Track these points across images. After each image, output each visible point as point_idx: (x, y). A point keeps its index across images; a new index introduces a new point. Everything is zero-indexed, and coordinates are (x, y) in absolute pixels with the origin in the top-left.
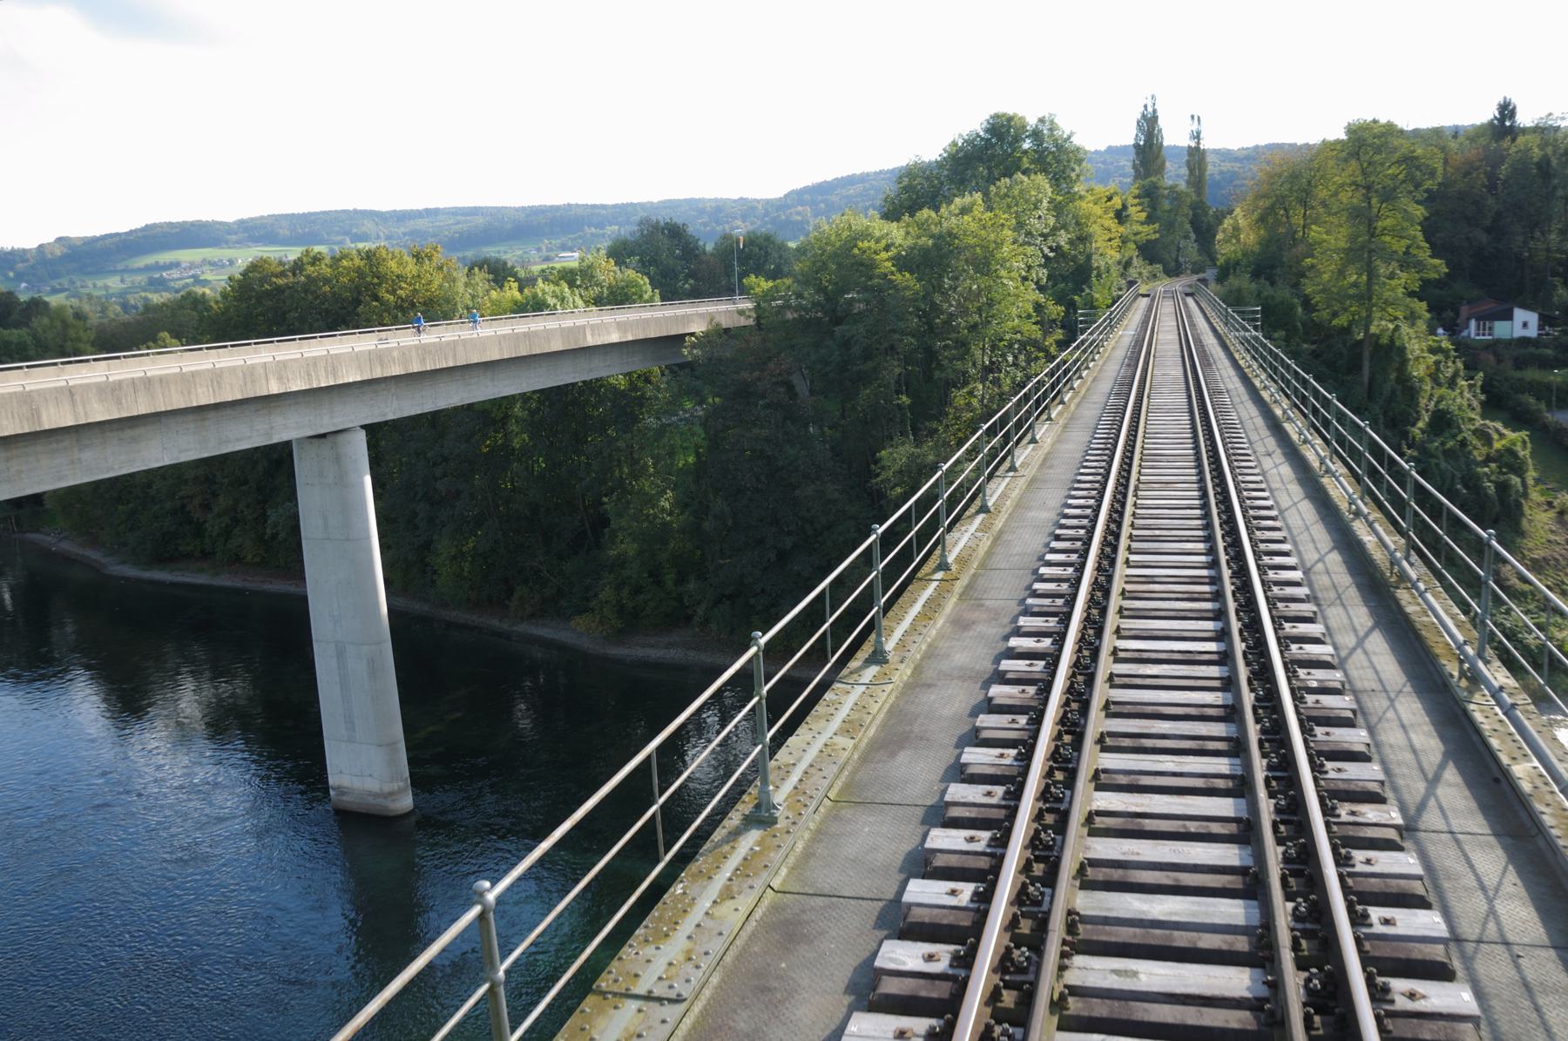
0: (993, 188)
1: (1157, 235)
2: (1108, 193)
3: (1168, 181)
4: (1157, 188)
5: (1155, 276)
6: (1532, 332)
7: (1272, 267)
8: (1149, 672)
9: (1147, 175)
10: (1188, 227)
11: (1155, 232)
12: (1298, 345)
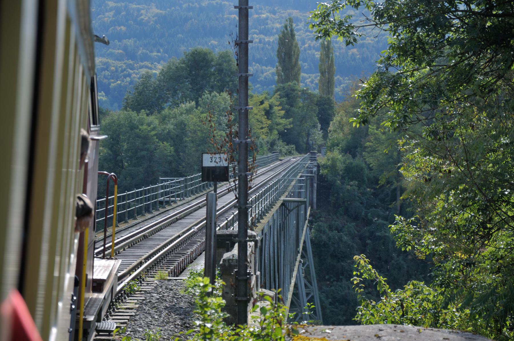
0: (200, 99)
1: (292, 126)
2: (261, 100)
3: (301, 86)
4: (294, 90)
5: (290, 152)
6: (103, 93)
7: (356, 147)
8: (283, 250)
9: (288, 78)
10: (316, 119)
11: (290, 124)
12: (365, 189)
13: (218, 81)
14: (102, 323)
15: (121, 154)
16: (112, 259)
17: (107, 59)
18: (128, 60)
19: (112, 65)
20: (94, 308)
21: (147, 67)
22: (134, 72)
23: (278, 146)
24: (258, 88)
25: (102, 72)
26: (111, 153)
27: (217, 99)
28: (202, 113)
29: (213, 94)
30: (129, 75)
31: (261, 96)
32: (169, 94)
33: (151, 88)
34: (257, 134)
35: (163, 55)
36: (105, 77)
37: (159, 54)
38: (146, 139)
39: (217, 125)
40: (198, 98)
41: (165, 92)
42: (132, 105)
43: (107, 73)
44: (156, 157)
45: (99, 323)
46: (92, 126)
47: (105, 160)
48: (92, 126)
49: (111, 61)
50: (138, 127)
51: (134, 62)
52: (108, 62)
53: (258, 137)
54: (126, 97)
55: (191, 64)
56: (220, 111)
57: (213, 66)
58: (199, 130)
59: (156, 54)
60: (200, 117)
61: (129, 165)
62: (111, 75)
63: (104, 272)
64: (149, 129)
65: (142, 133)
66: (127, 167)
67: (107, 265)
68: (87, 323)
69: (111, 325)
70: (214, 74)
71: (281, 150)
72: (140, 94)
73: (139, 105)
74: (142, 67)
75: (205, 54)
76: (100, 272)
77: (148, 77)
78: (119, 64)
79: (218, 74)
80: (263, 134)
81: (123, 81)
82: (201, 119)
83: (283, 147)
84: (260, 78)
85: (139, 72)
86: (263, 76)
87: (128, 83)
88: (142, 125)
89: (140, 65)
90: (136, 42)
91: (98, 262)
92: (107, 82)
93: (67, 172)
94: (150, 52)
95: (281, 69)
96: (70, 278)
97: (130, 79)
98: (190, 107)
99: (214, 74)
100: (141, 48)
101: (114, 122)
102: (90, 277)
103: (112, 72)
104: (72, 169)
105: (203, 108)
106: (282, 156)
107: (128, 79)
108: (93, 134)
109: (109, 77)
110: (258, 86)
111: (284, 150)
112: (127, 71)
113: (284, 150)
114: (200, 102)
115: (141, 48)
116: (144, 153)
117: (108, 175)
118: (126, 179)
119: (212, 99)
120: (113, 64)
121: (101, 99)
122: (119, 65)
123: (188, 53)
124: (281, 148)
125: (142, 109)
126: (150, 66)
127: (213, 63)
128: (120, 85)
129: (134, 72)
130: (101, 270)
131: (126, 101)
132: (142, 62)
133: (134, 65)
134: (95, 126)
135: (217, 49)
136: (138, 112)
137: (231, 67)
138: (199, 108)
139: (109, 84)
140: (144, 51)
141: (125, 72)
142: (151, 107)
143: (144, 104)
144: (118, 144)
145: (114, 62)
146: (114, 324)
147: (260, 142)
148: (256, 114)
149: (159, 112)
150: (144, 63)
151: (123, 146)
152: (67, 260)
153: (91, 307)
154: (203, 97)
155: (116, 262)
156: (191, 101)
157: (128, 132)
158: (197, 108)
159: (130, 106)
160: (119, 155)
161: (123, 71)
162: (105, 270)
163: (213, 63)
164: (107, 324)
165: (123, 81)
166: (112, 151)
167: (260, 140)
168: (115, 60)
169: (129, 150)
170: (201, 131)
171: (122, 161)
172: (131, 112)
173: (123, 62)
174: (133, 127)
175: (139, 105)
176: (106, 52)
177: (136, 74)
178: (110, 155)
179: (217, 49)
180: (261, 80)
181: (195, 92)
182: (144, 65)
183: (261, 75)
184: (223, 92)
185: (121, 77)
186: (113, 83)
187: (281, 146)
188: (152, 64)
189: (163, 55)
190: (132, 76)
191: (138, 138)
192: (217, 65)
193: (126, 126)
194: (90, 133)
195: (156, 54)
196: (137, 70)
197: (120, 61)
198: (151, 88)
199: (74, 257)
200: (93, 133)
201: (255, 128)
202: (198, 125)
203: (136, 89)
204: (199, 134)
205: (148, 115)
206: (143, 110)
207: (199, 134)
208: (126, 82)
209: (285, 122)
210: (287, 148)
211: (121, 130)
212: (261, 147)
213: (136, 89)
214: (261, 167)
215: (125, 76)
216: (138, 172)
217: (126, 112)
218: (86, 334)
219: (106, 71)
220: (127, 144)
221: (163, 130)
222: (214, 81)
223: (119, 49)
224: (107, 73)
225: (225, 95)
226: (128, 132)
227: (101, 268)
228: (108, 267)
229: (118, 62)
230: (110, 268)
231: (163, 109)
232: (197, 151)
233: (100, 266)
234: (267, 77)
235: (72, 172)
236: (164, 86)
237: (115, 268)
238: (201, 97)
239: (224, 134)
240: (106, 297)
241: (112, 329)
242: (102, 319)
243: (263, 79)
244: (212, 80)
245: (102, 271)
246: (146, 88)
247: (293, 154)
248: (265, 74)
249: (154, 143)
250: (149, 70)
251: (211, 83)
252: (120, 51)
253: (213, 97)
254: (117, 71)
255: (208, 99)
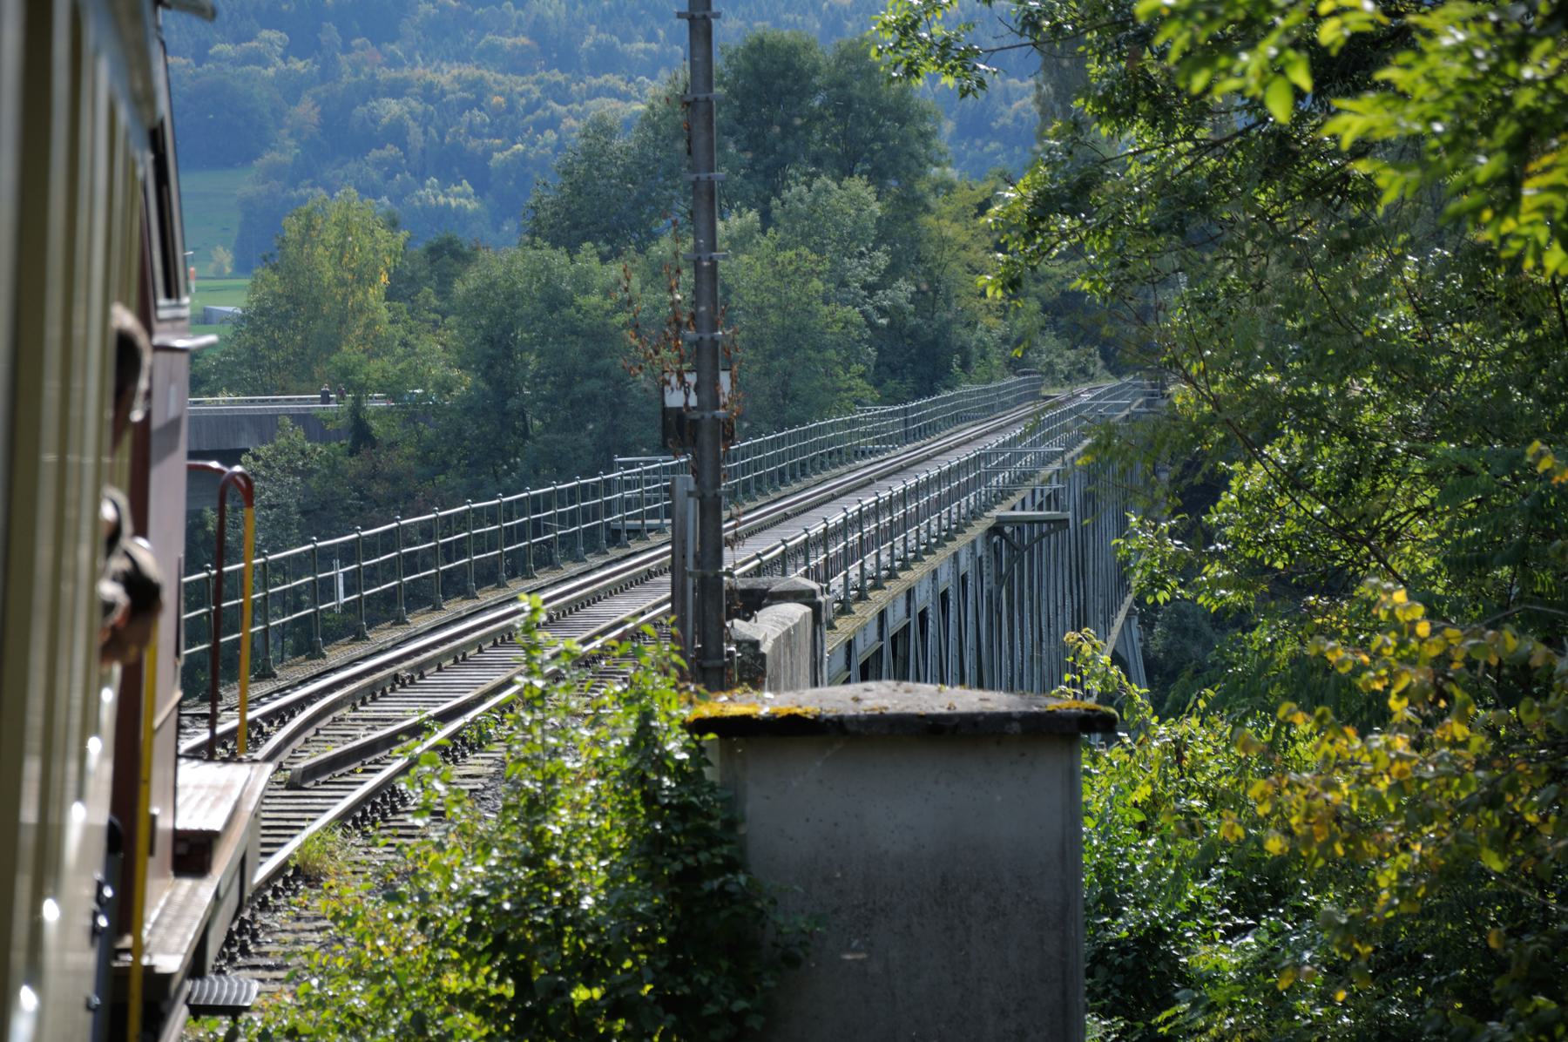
0: (775, 202)
2: (980, 199)
13: (835, 140)
14: (207, 984)
15: (521, 391)
16: (240, 761)
17: (478, 68)
18: (548, 68)
19: (496, 88)
20: (181, 930)
21: (613, 93)
22: (570, 111)
23: (1040, 352)
24: (994, 153)
25: (461, 113)
26: (487, 388)
27: (832, 201)
28: (782, 246)
29: (817, 184)
30: (553, 123)
31: (981, 187)
32: (674, 187)
33: (614, 170)
34: (967, 313)
35: (668, 50)
36: (473, 132)
37: (654, 46)
38: (598, 338)
39: (831, 285)
40: (767, 201)
41: (661, 179)
42: (552, 226)
43: (478, 116)
44: (635, 397)
45: (198, 983)
46: (162, 301)
47: (468, 410)
48: (162, 301)
49: (490, 75)
50: (572, 302)
51: (568, 75)
52: (482, 78)
53: (971, 325)
54: (531, 202)
55: (743, 87)
56: (840, 240)
57: (817, 90)
58: (771, 306)
59: (642, 45)
60: (774, 263)
61: (547, 427)
62: (492, 124)
63: (214, 806)
64: (608, 304)
65: (587, 321)
66: (540, 434)
67: (222, 782)
68: (158, 984)
69: (240, 988)
70: (821, 117)
71: (1050, 365)
72: (577, 189)
73: (575, 226)
74: (596, 93)
75: (792, 51)
76: (198, 806)
77: (602, 129)
78: (521, 84)
79: (835, 115)
80: (989, 311)
81: (534, 144)
82: (779, 267)
83: (1060, 356)
84: (1001, 121)
85: (586, 111)
86: (1011, 112)
87: (548, 150)
88: (586, 292)
89: (589, 87)
90: (575, 8)
91: (190, 772)
92: (480, 150)
93: (62, 464)
94: (622, 42)
95: (1051, 90)
96: (88, 829)
97: (555, 136)
98: (742, 229)
99: (821, 117)
100: (593, 28)
101: (492, 285)
102: (164, 824)
103: (496, 113)
104: (82, 453)
105: (786, 230)
106: (1054, 385)
107: (551, 136)
108: (165, 332)
109: (486, 130)
110: (993, 146)
111: (1062, 366)
112: (546, 108)
113: (1062, 366)
114: (776, 213)
115: (593, 28)
116: (594, 385)
117: (220, 472)
118: (536, 472)
119: (815, 201)
120: (499, 83)
121: (459, 207)
122: (519, 89)
123: (733, 48)
124: (1052, 356)
125: (585, 240)
126: (623, 87)
127: (817, 81)
128: (522, 159)
129: (570, 111)
130: (203, 799)
131: (533, 214)
132: (596, 76)
133: (568, 88)
134: (173, 302)
135: (850, 25)
136: (573, 250)
137: (879, 94)
138: (771, 230)
139: (488, 154)
140: (603, 37)
141: (539, 112)
142: (616, 232)
143: (593, 223)
144: (509, 357)
145: (500, 77)
146: (249, 985)
147: (980, 340)
148: (964, 247)
149: (641, 250)
150: (601, 80)
151: (526, 365)
152: (73, 767)
153: (170, 928)
154: (786, 194)
155: (254, 773)
156: (744, 210)
157: (539, 319)
158: (764, 231)
159: (545, 231)
160: (512, 394)
161: (531, 108)
162: (219, 799)
163: (817, 81)
164: (226, 984)
165: (534, 144)
166: (489, 382)
167: (979, 334)
168: (505, 73)
169: (545, 376)
170: (782, 309)
171: (522, 414)
172: (547, 251)
173: (534, 78)
174: (555, 301)
175: (575, 226)
176: (474, 44)
177: (577, 119)
178: (484, 395)
179: (850, 25)
180: (1004, 127)
181: (761, 177)
182: (601, 87)
183: (1003, 108)
184: (851, 176)
185: (526, 130)
186: (501, 149)
187: (1056, 352)
188: (630, 80)
189: (668, 50)
190: (562, 127)
191: (574, 338)
192: (830, 85)
193: (533, 298)
194: (157, 327)
195: (642, 45)
196: (581, 104)
197: (522, 74)
198: (614, 170)
199: (102, 755)
200: (167, 326)
201: (962, 292)
202: (768, 290)
203: (565, 173)
204: (774, 317)
205: (604, 259)
206: (587, 245)
207: (774, 317)
208: (543, 147)
209: (1064, 271)
210: (1073, 358)
211: (518, 311)
212: (982, 357)
213: (565, 173)
214: (970, 419)
215: (541, 127)
216: (574, 449)
217: (531, 253)
218: (155, 1019)
219: (476, 111)
220: (538, 356)
221: (656, 309)
222: (823, 139)
223: (516, 34)
224: (478, 116)
225: (858, 185)
226: (539, 319)
227: (203, 792)
228: (227, 788)
229: (515, 78)
230: (235, 795)
231: (653, 237)
232: (768, 373)
233: (198, 787)
234: (1023, 115)
235: (81, 466)
236: (658, 160)
237: (251, 792)
238: (778, 196)
239: (854, 314)
240: (222, 893)
241: (246, 999)
242: (209, 968)
243: (1009, 121)
244: (817, 137)
245: (207, 804)
246: (598, 169)
247: (1092, 377)
248: (1017, 105)
249: (628, 352)
250: (620, 104)
251: (813, 148)
252: (523, 40)
253: (818, 193)
254: (511, 109)
255: (801, 200)
